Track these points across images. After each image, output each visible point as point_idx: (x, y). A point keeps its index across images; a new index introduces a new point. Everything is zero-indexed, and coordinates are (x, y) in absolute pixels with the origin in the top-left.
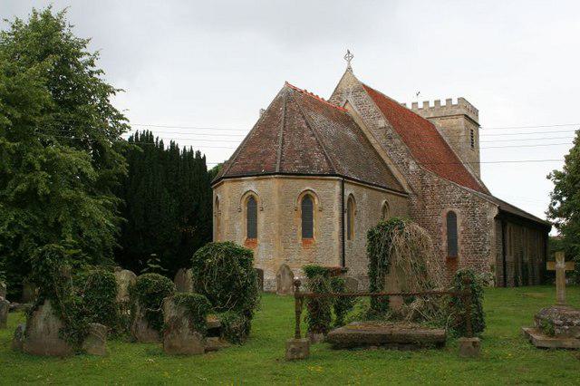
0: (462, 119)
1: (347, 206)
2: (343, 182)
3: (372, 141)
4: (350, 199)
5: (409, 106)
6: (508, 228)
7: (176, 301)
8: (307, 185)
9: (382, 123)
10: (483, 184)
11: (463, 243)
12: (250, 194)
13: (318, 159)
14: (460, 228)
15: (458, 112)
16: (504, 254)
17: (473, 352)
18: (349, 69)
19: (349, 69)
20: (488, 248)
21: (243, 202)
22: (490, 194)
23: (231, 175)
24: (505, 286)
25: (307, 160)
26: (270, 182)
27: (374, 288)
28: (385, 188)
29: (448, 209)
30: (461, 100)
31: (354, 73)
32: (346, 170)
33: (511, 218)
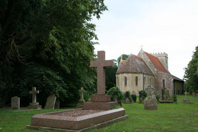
0: (164, 57)
1: (144, 79)
2: (143, 74)
3: (147, 64)
5: (152, 54)
8: (136, 75)
9: (149, 60)
13: (138, 69)
14: (165, 83)
15: (164, 55)
16: (175, 88)
18: (142, 49)
19: (142, 49)
22: (170, 74)
25: (136, 70)
30: (164, 53)
32: (143, 72)
33: (176, 81)
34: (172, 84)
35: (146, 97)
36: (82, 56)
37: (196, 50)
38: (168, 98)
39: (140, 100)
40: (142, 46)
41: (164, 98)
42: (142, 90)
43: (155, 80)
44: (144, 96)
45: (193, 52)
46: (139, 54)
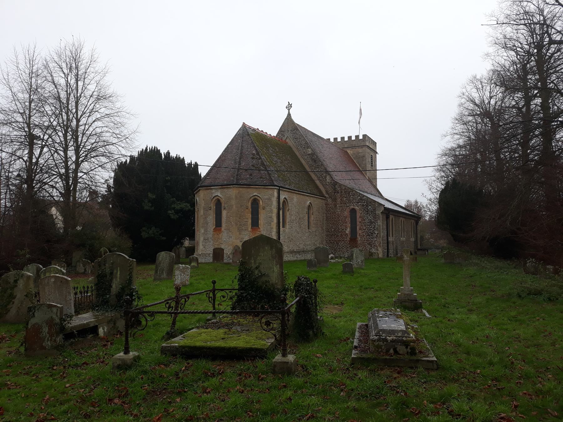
2: (279, 190)
4: (284, 201)
12: (217, 197)
14: (359, 220)
18: (289, 115)
19: (289, 115)
26: (230, 190)
40: (289, 106)
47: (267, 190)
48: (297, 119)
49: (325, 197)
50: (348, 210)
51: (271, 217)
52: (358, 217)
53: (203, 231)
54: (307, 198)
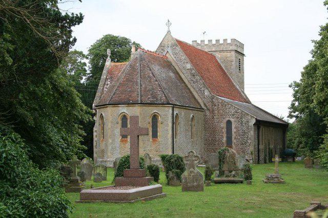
0: (233, 53)
2: (173, 107)
3: (183, 76)
4: (176, 116)
6: (261, 129)
7: (173, 172)
9: (189, 66)
10: (246, 96)
11: (235, 138)
12: (124, 114)
13: (160, 95)
14: (234, 130)
15: (231, 48)
16: (258, 145)
17: (250, 183)
18: (169, 32)
19: (169, 32)
20: (249, 142)
21: (119, 118)
22: (248, 102)
23: (112, 103)
24: (258, 163)
26: (135, 108)
27: (220, 168)
28: (192, 107)
29: (227, 119)
30: (234, 40)
31: (171, 34)
32: (173, 100)
33: (268, 126)
34: (252, 133)
35: (182, 170)
36: (57, 90)
37: (320, 35)
38: (233, 173)
39: (167, 177)
40: (169, 23)
41: (224, 172)
42: (170, 154)
43: (206, 121)
44: (178, 168)
45: (313, 41)
46: (161, 46)
47: (164, 108)
48: (258, 118)
49: (204, 109)
50: (225, 121)
51: (167, 130)
52: (233, 127)
53: (111, 141)
54: (191, 111)
